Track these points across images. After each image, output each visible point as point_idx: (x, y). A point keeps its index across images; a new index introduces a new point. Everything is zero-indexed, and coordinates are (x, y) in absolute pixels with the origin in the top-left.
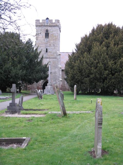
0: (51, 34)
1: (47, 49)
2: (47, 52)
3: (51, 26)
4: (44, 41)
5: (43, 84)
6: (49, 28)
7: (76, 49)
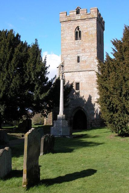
0: (84, 32)
1: (78, 57)
2: (78, 61)
3: (85, 19)
4: (73, 45)
5: (73, 115)
6: (80, 24)
7: (97, 71)
